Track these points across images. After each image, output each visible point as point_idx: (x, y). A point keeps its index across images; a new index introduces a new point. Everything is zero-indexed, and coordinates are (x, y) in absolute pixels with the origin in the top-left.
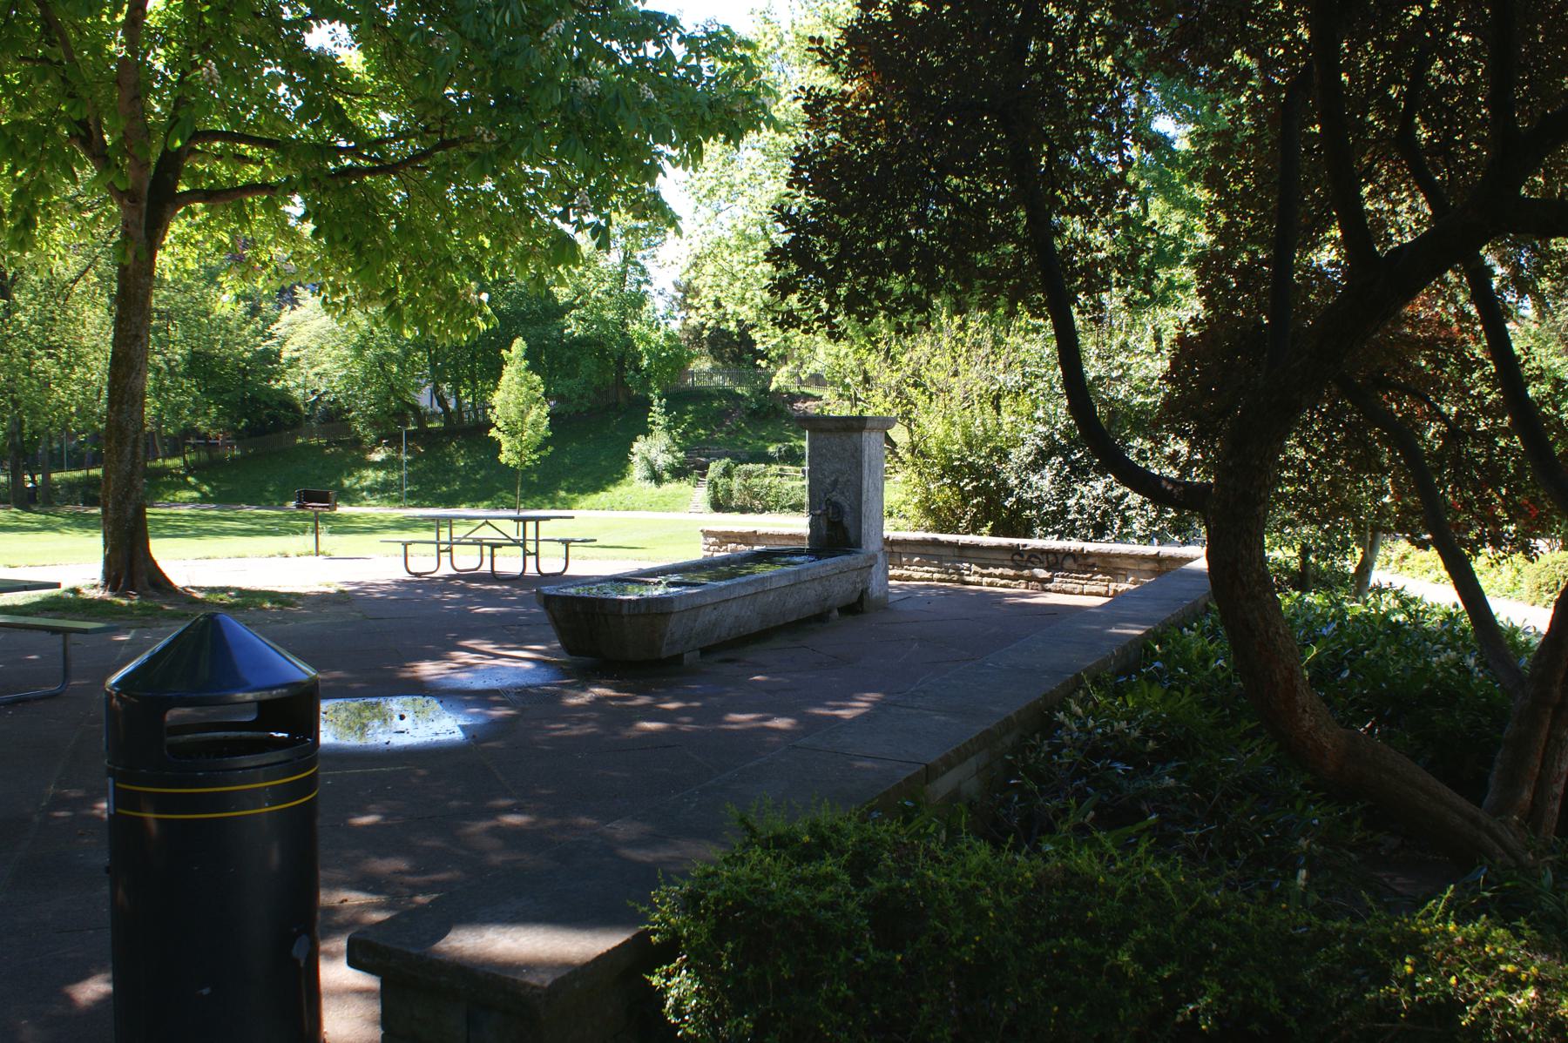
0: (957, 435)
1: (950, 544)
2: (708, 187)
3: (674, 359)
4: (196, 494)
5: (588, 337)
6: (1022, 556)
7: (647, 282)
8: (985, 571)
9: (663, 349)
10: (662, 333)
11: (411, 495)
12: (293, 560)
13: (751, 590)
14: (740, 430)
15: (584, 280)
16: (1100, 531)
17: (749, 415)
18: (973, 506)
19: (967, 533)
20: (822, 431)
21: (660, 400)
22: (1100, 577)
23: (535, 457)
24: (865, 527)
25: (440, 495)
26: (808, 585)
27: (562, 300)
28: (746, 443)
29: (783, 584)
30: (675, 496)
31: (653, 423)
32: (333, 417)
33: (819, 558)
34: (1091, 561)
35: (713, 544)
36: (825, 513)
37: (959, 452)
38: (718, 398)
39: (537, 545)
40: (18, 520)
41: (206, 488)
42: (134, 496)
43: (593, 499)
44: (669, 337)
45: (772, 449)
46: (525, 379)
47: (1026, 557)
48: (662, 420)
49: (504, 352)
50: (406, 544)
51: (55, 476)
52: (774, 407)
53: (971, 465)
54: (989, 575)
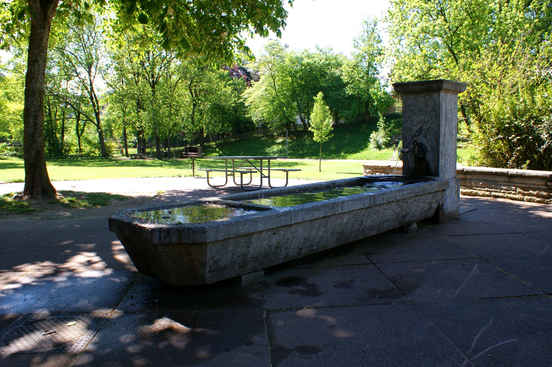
0: (508, 110)
1: (502, 174)
2: (396, 29)
3: (387, 102)
4: (218, 154)
5: (354, 95)
7: (378, 74)
8: (526, 192)
9: (383, 98)
10: (382, 92)
11: (289, 154)
12: (183, 178)
13: (319, 214)
15: (353, 73)
18: (518, 151)
19: (514, 168)
20: (411, 93)
21: (383, 117)
23: (327, 138)
24: (442, 161)
25: (300, 154)
26: (385, 207)
27: (345, 81)
29: (357, 206)
30: (385, 154)
32: (264, 126)
33: (409, 183)
36: (412, 151)
37: (509, 118)
39: (269, 172)
40: (154, 162)
41: (221, 152)
42: (35, 145)
43: (354, 155)
44: (385, 93)
46: (323, 107)
48: (382, 125)
49: (314, 97)
51: (172, 149)
53: (516, 127)
54: (529, 195)
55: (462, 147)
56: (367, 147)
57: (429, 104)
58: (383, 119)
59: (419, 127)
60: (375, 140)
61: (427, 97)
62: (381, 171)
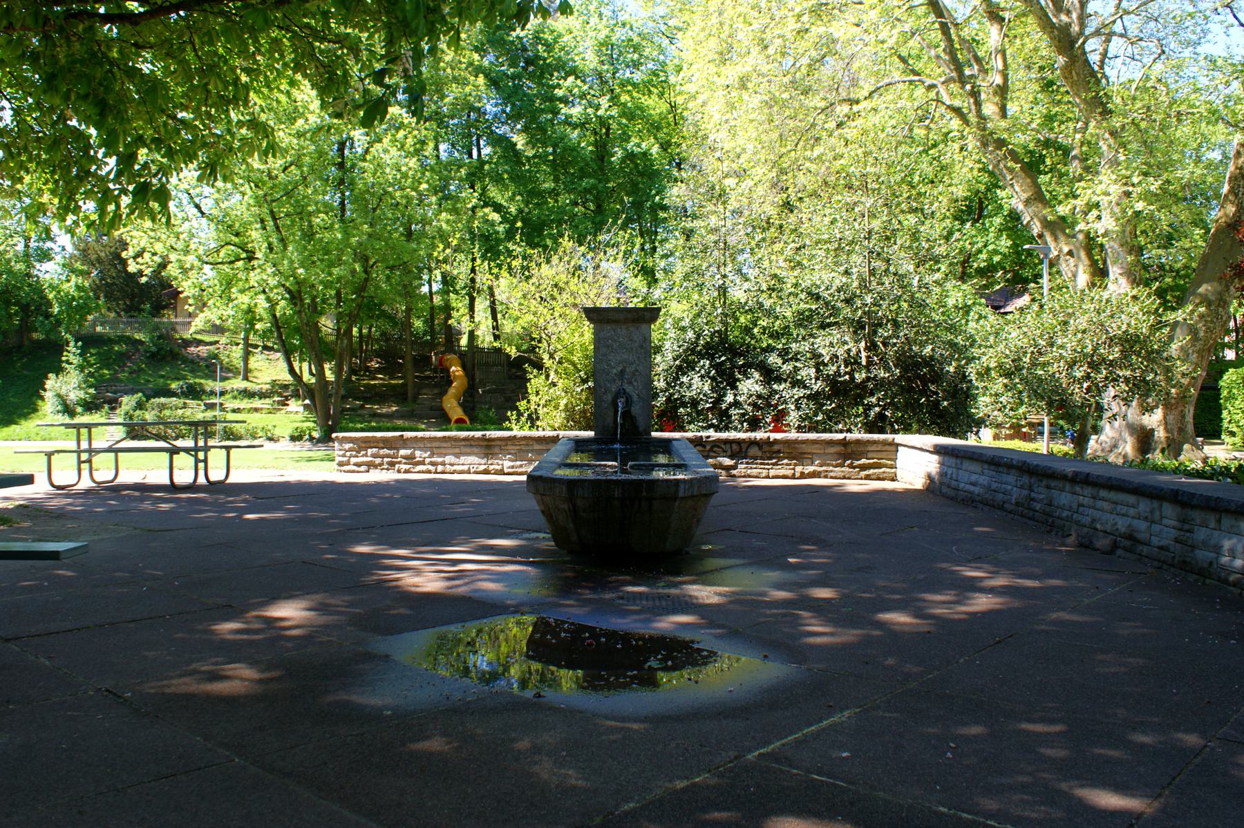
6: (704, 447)
9: (73, 299)
14: (140, 370)
16: (754, 424)
17: (148, 358)
20: (608, 321)
21: (76, 342)
22: (785, 461)
28: (149, 381)
31: (68, 362)
34: (776, 447)
35: (350, 450)
38: (117, 343)
45: (174, 385)
47: (708, 447)
48: (76, 360)
50: (49, 455)
52: (171, 351)
55: (262, 409)
56: (35, 410)
57: (635, 338)
58: (75, 346)
59: (619, 369)
60: (59, 396)
61: (631, 329)
62: (381, 445)
